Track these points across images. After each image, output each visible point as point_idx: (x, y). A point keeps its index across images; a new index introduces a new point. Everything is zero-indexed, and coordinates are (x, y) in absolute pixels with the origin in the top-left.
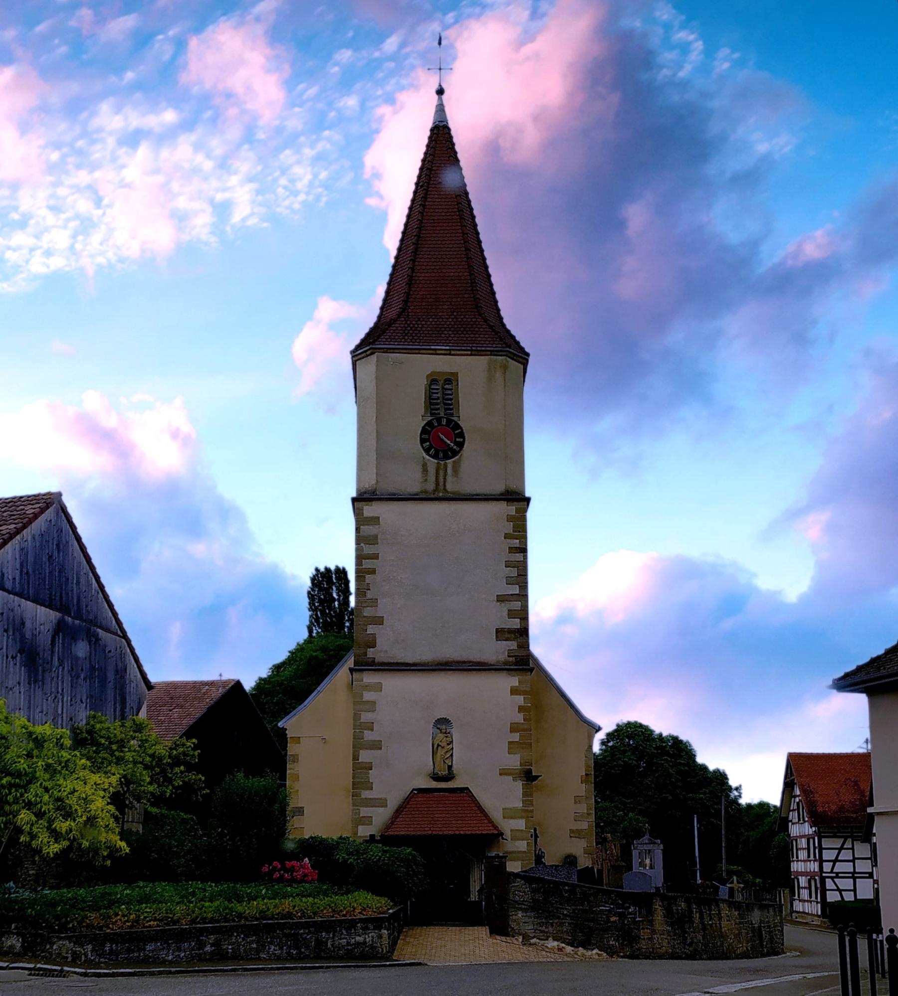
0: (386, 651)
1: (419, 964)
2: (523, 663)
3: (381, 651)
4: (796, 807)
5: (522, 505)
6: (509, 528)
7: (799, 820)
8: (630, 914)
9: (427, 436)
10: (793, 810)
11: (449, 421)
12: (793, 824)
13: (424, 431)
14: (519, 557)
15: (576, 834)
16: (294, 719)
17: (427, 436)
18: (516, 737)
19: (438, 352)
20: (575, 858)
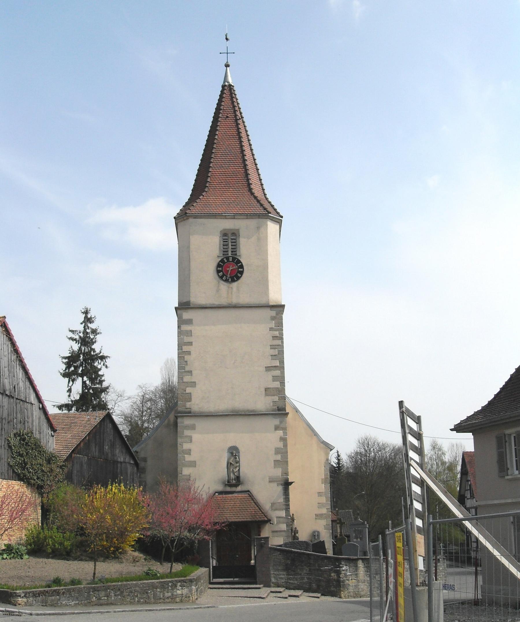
0: (197, 404)
1: (214, 607)
2: (280, 411)
3: (194, 404)
4: (469, 488)
5: (281, 309)
6: (273, 324)
7: (471, 497)
8: (343, 570)
9: (220, 269)
10: (467, 490)
11: (234, 259)
12: (468, 499)
13: (219, 266)
14: (278, 342)
15: (318, 516)
16: (167, 613)
17: (220, 269)
18: (279, 457)
19: (227, 217)
20: (318, 532)
